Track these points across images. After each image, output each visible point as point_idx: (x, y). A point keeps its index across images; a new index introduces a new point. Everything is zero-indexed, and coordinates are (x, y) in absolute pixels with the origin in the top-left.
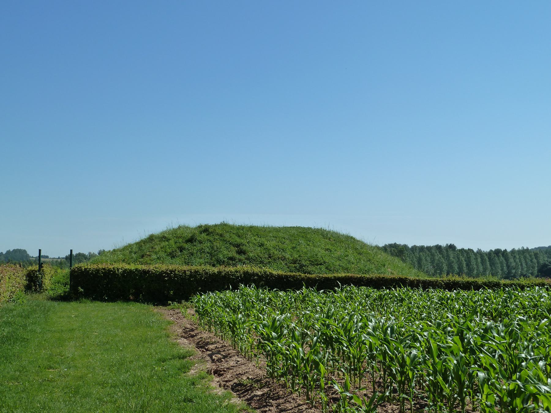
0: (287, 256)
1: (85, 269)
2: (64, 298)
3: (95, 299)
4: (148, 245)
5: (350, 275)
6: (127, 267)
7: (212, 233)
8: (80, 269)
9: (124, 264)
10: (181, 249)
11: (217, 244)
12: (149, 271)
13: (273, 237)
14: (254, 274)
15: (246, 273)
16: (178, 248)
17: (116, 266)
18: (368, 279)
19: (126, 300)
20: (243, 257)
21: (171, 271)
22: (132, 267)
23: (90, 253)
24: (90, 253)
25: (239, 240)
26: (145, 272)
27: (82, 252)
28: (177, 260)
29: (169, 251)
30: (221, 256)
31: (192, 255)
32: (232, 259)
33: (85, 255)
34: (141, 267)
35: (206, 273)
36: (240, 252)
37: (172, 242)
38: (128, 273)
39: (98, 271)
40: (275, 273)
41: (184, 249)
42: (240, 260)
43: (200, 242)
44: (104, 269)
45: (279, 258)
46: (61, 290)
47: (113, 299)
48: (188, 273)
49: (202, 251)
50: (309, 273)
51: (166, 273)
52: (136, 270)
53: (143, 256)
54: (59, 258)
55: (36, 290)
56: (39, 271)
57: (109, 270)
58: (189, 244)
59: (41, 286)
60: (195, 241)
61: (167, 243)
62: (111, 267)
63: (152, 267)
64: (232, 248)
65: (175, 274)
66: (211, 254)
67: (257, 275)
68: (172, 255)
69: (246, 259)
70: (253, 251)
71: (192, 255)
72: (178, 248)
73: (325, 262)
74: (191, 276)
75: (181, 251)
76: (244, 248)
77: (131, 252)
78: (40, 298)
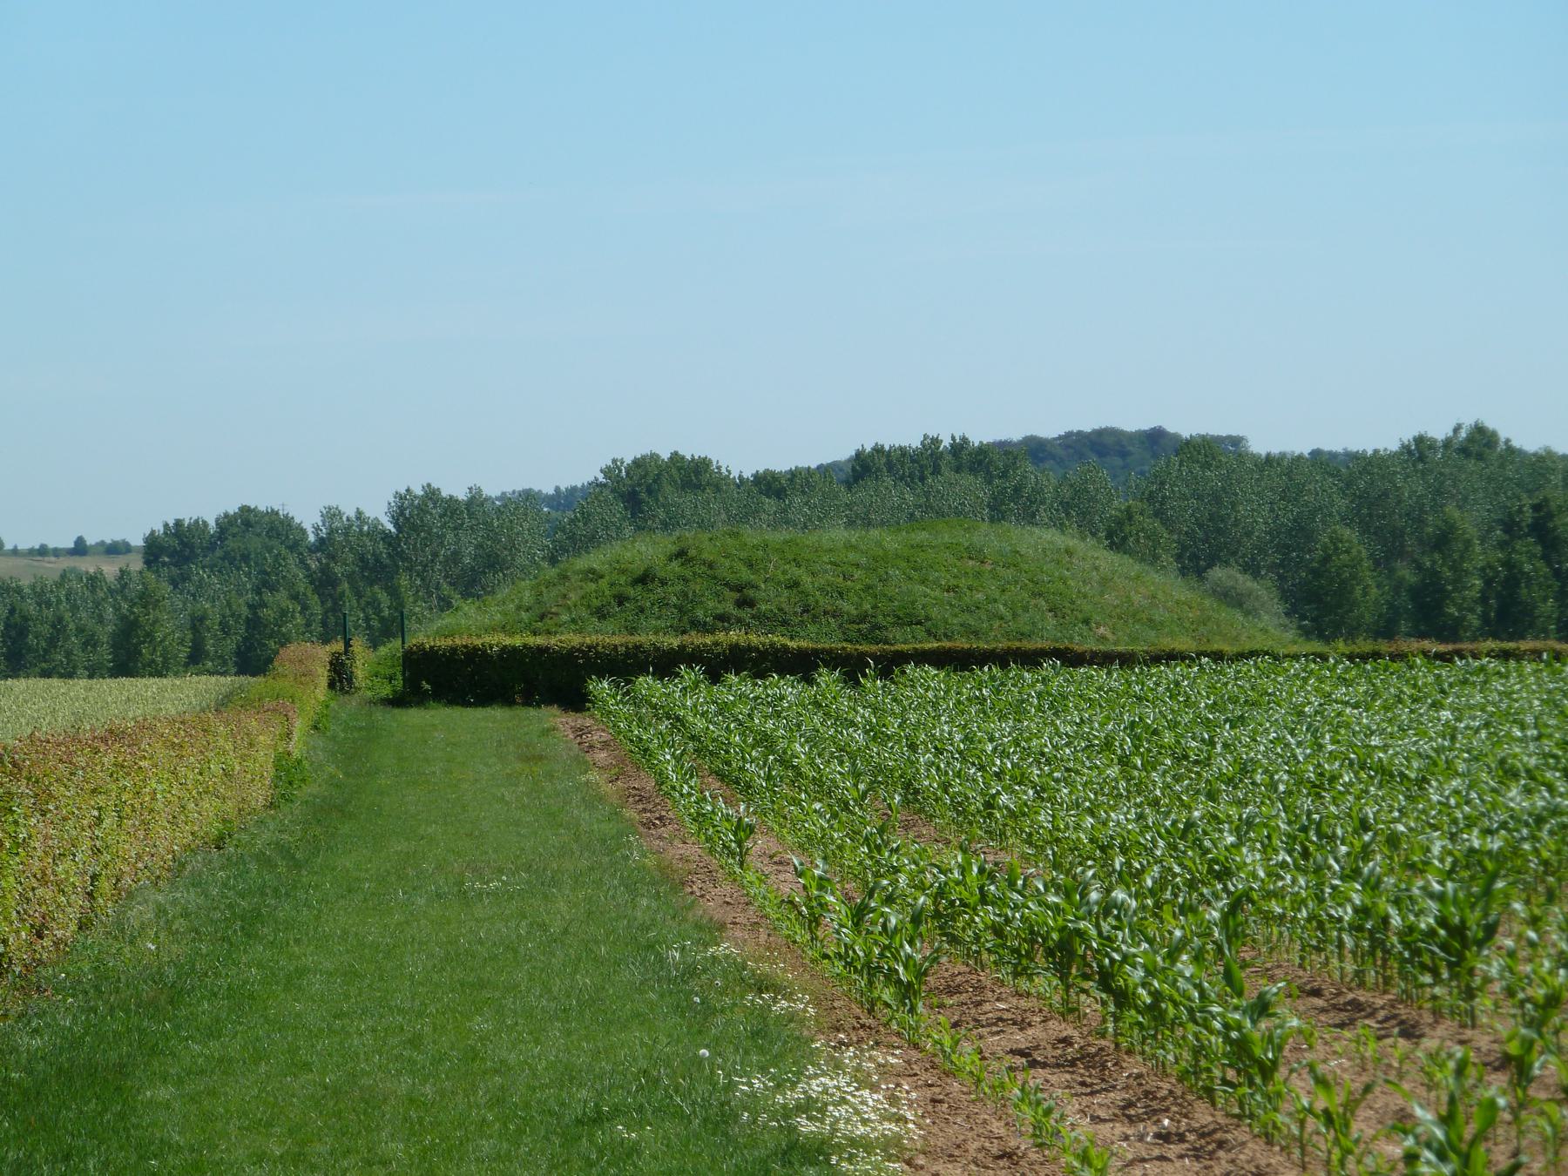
0: (847, 607)
1: (432, 648)
2: (398, 701)
3: (452, 702)
4: (554, 592)
5: (947, 644)
6: (508, 641)
7: (692, 559)
8: (421, 647)
9: (502, 636)
10: (621, 600)
11: (697, 587)
12: (547, 649)
13: (831, 563)
14: (750, 649)
15: (734, 647)
16: (615, 597)
17: (487, 639)
18: (985, 651)
19: (509, 702)
20: (746, 614)
21: (590, 647)
22: (517, 641)
23: (331, 514)
24: (331, 514)
25: (745, 575)
26: (541, 650)
27: (262, 502)
28: (609, 625)
29: (596, 603)
30: (700, 613)
31: (642, 611)
32: (722, 618)
33: (287, 522)
34: (540, 641)
35: (657, 649)
36: (744, 603)
37: (603, 583)
38: (510, 654)
39: (454, 650)
40: (792, 644)
41: (627, 599)
42: (739, 620)
43: (663, 583)
44: (466, 647)
45: (826, 613)
46: (386, 691)
47: (484, 700)
48: (622, 650)
49: (663, 603)
50: (886, 642)
51: (579, 650)
52: (525, 646)
53: (542, 617)
54: (80, 548)
55: (342, 689)
56: (346, 652)
57: (476, 649)
58: (639, 588)
59: (350, 681)
60: (653, 580)
61: (593, 586)
62: (478, 642)
63: (553, 641)
64: (727, 593)
65: (597, 653)
66: (680, 609)
67: (757, 649)
68: (601, 614)
69: (753, 617)
70: (770, 599)
71: (642, 611)
72: (615, 597)
73: (928, 618)
74: (627, 655)
75: (620, 604)
76: (751, 593)
77: (519, 608)
78: (353, 702)
